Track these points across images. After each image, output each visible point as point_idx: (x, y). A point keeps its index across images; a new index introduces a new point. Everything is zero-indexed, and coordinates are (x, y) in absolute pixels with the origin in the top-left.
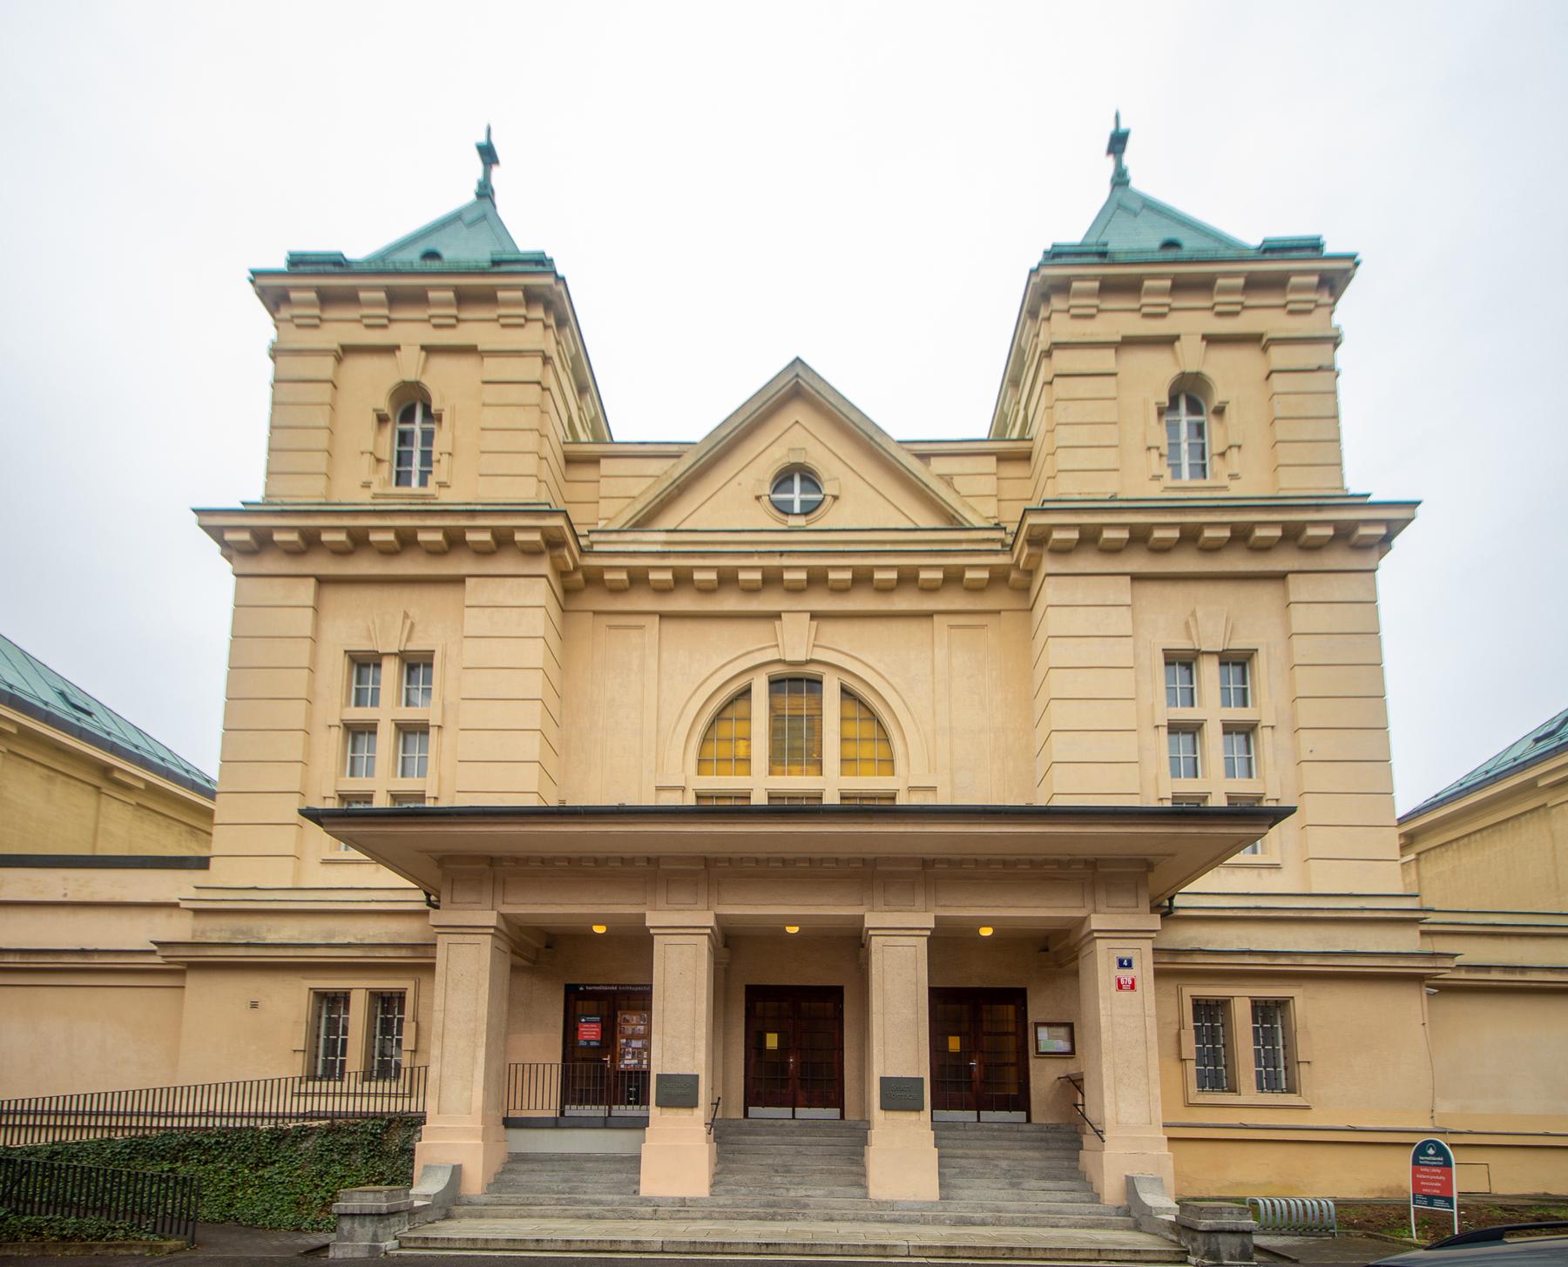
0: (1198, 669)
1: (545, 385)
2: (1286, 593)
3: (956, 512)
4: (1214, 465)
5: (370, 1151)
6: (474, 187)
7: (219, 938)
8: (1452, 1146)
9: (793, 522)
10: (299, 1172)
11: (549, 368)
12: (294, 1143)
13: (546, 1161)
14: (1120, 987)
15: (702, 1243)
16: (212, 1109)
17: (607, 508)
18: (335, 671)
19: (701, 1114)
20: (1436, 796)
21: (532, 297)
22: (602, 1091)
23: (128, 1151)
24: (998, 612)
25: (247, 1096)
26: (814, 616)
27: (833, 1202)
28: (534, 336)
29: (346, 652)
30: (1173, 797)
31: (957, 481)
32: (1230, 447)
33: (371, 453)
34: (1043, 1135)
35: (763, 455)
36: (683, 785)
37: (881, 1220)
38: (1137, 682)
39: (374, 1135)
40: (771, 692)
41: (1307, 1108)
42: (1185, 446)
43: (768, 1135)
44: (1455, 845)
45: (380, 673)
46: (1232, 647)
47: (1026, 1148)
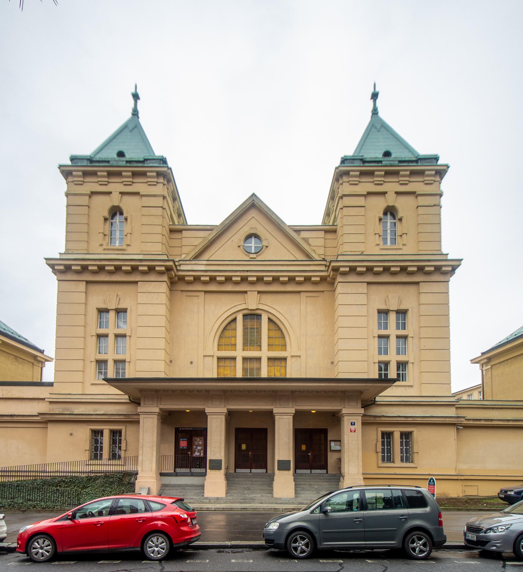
1: (164, 207)
2: (419, 290)
3: (309, 253)
4: (398, 239)
5: (118, 483)
7: (59, 411)
9: (252, 256)
10: (97, 490)
11: (165, 200)
12: (94, 481)
13: (173, 486)
14: (351, 431)
15: (226, 508)
16: (58, 469)
17: (185, 250)
18: (93, 314)
19: (223, 471)
20: (500, 342)
21: (159, 174)
22: (186, 464)
23: (42, 483)
24: (323, 291)
25: (72, 465)
26: (259, 292)
27: (263, 498)
28: (159, 189)
29: (97, 308)
30: (379, 362)
31: (311, 241)
32: (403, 234)
33: (103, 233)
34: (330, 477)
35: (241, 230)
36: (213, 355)
38: (368, 321)
39: (119, 478)
40: (243, 319)
41: (416, 468)
42: (389, 231)
43: (242, 478)
44: (503, 363)
45: (109, 315)
46: (400, 308)
47: (324, 482)
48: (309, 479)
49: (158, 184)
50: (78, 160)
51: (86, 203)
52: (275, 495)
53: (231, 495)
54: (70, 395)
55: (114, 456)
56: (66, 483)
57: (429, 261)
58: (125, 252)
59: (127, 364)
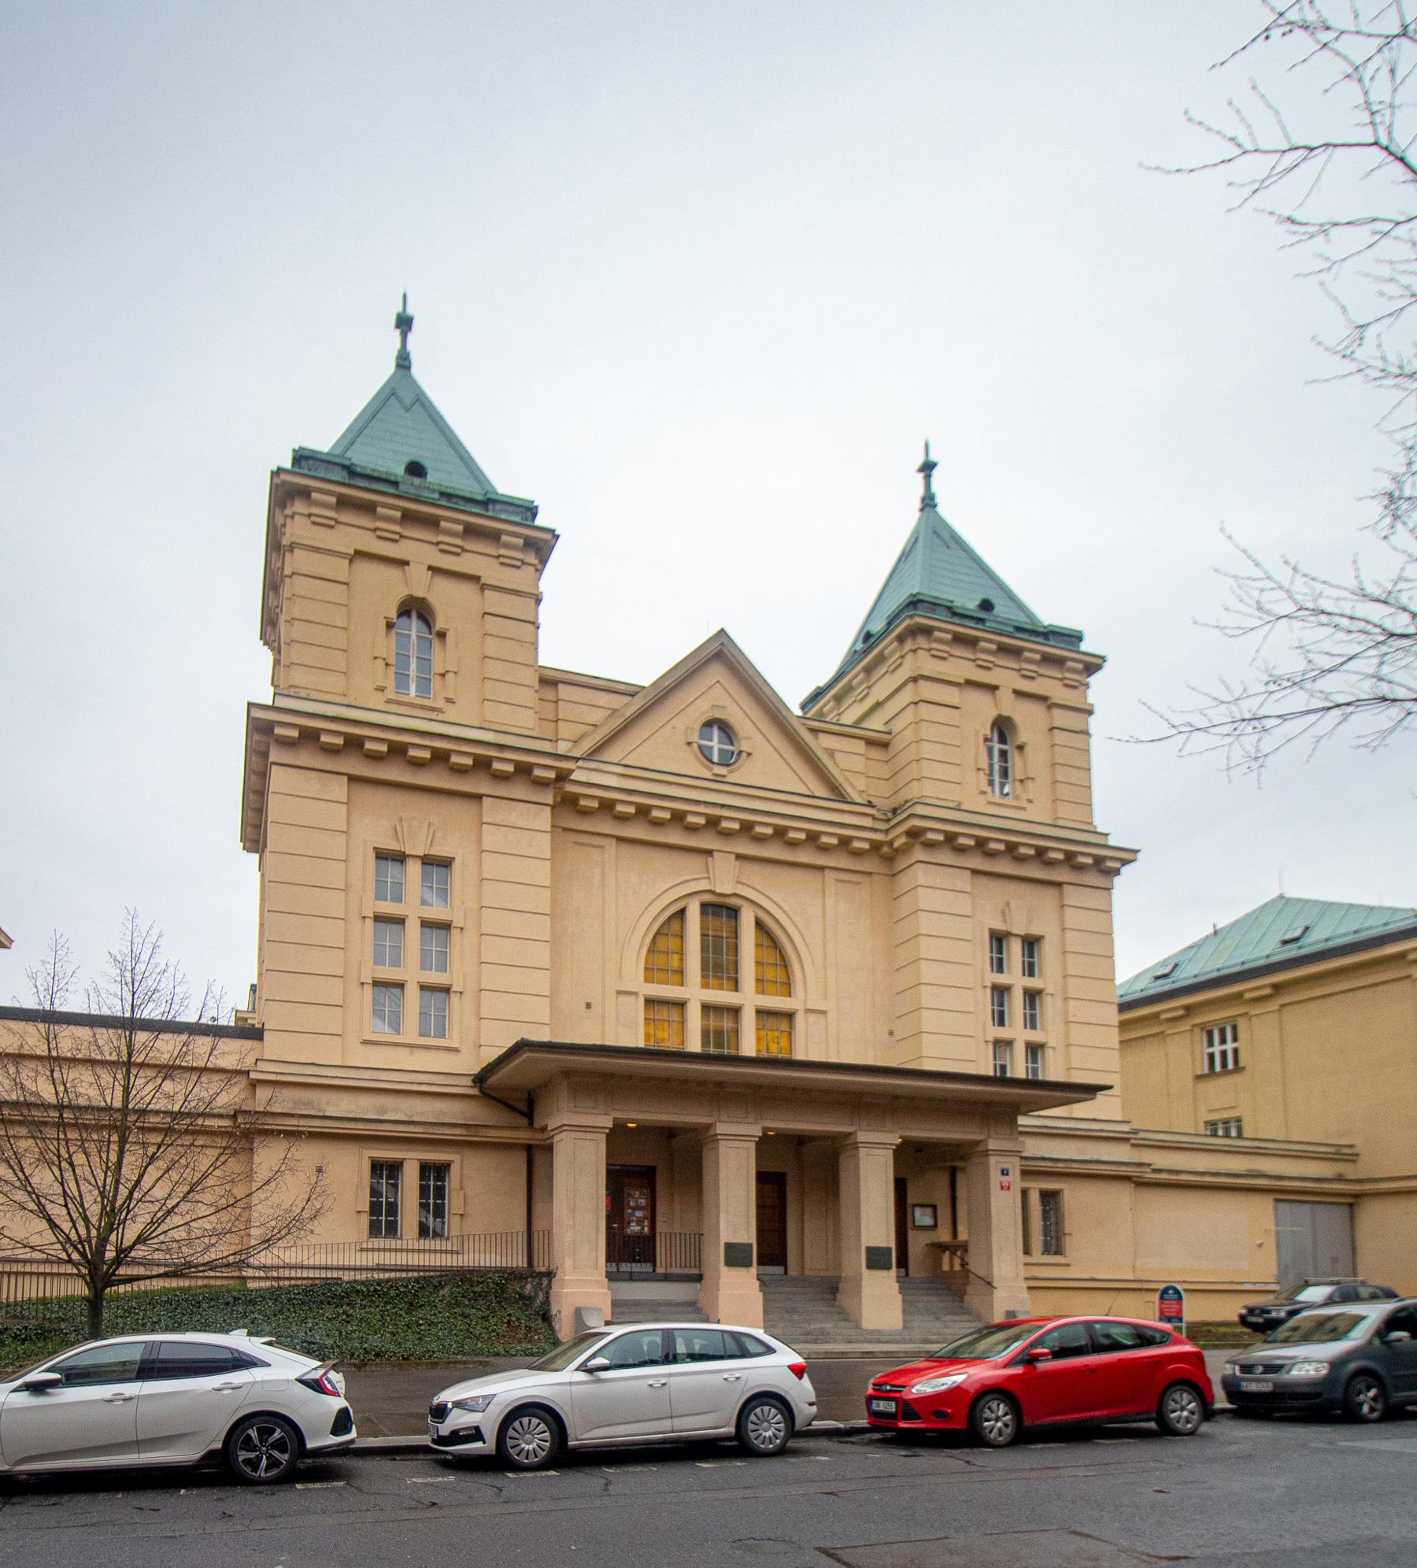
0: (1008, 945)
2: (1061, 897)
4: (436, 682)
7: (283, 1107)
8: (1185, 1290)
14: (1002, 1188)
26: (739, 857)
30: (374, 982)
31: (838, 756)
33: (384, 659)
41: (1068, 1265)
50: (317, 463)
57: (1086, 844)
59: (455, 998)
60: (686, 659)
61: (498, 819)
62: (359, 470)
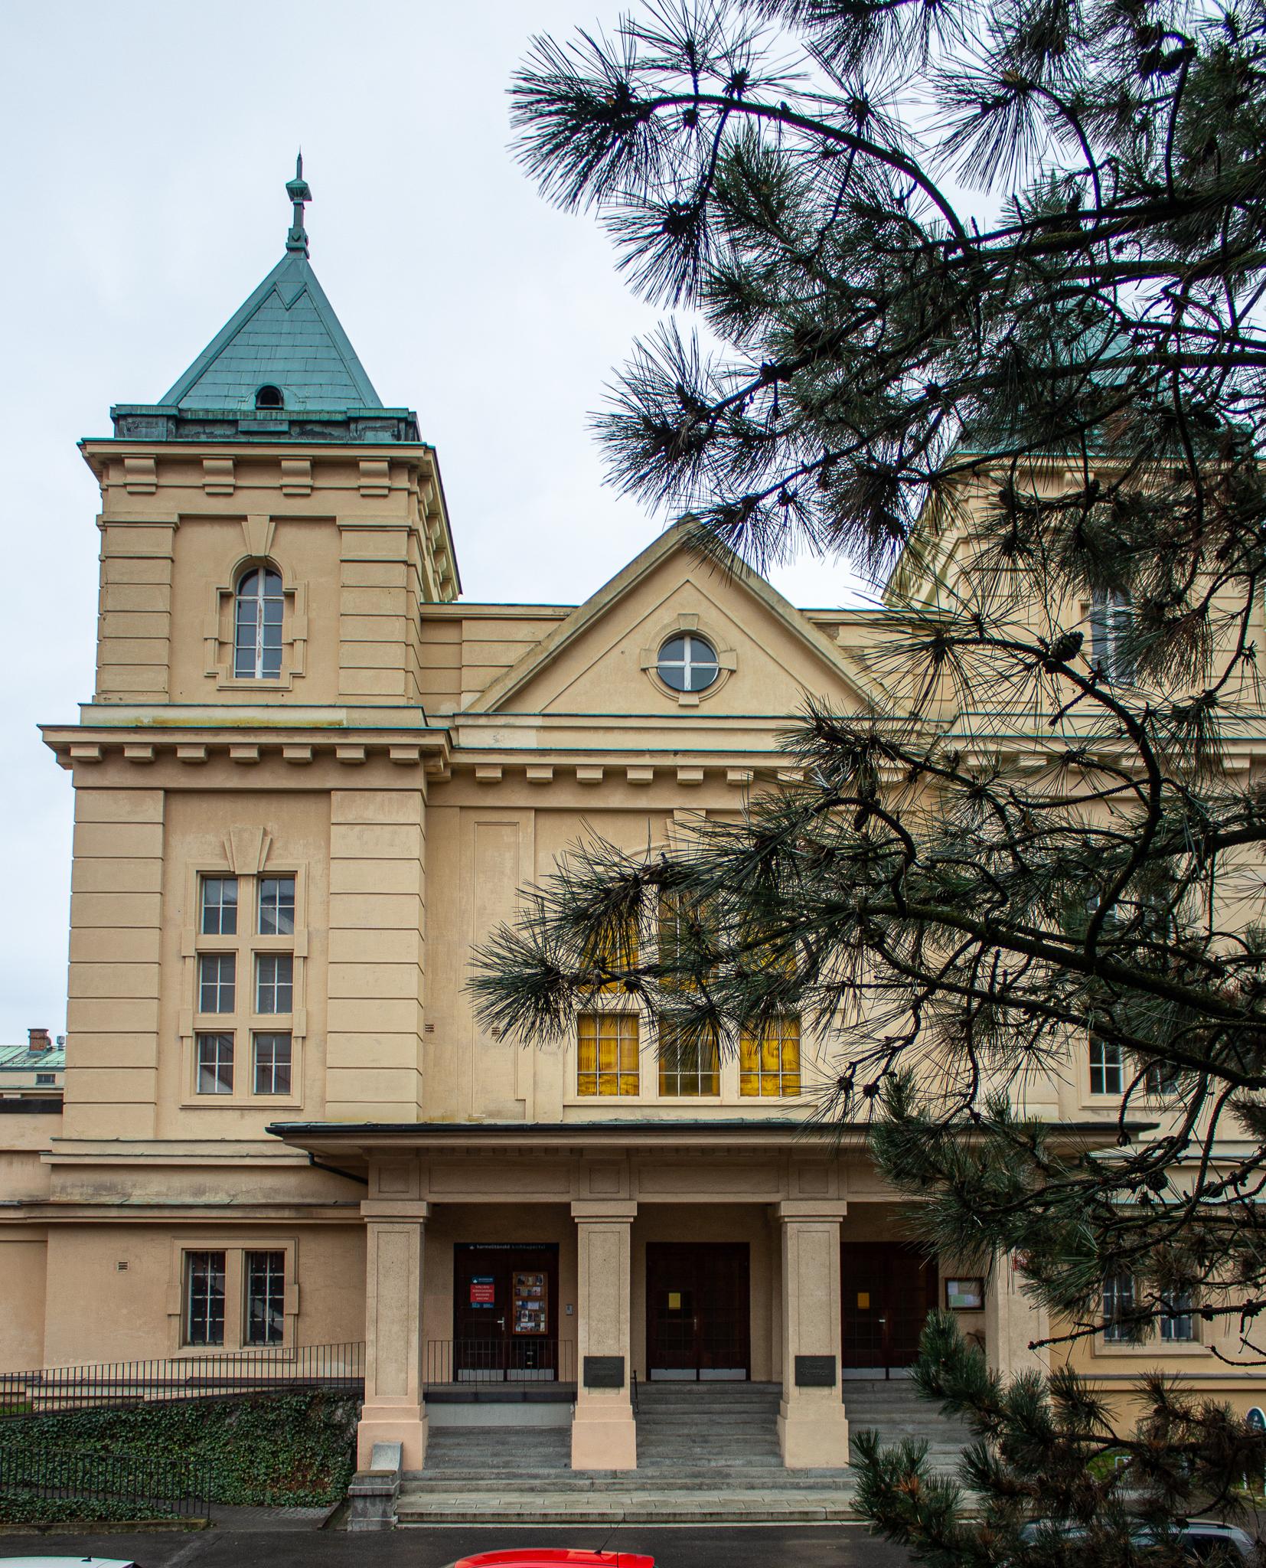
6: (284, 238)
11: (414, 539)
18: (187, 898)
19: (626, 1391)
22: (493, 1355)
28: (400, 509)
37: (797, 1487)
48: (885, 1401)
49: (393, 493)
51: (166, 550)
52: (791, 1461)
53: (653, 1464)
54: (116, 1144)
55: (257, 1332)
56: (132, 1428)
58: (288, 699)
60: (635, 561)
61: (341, 820)
62: (189, 416)
